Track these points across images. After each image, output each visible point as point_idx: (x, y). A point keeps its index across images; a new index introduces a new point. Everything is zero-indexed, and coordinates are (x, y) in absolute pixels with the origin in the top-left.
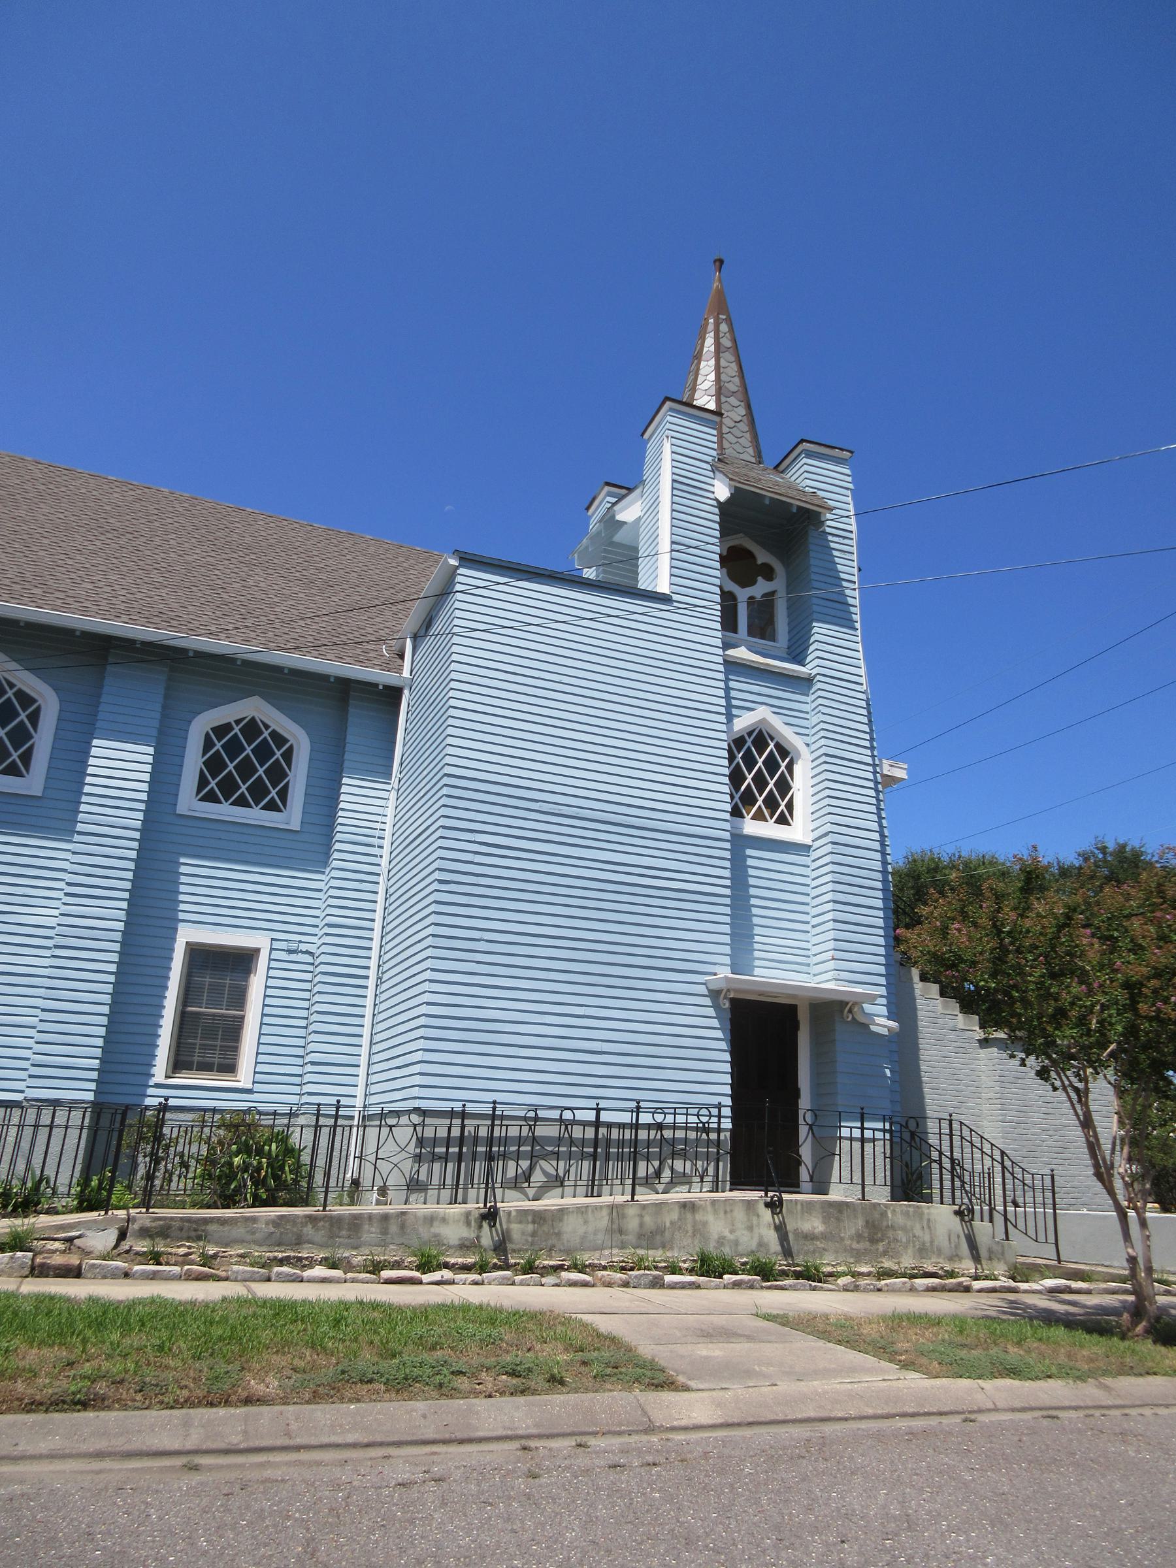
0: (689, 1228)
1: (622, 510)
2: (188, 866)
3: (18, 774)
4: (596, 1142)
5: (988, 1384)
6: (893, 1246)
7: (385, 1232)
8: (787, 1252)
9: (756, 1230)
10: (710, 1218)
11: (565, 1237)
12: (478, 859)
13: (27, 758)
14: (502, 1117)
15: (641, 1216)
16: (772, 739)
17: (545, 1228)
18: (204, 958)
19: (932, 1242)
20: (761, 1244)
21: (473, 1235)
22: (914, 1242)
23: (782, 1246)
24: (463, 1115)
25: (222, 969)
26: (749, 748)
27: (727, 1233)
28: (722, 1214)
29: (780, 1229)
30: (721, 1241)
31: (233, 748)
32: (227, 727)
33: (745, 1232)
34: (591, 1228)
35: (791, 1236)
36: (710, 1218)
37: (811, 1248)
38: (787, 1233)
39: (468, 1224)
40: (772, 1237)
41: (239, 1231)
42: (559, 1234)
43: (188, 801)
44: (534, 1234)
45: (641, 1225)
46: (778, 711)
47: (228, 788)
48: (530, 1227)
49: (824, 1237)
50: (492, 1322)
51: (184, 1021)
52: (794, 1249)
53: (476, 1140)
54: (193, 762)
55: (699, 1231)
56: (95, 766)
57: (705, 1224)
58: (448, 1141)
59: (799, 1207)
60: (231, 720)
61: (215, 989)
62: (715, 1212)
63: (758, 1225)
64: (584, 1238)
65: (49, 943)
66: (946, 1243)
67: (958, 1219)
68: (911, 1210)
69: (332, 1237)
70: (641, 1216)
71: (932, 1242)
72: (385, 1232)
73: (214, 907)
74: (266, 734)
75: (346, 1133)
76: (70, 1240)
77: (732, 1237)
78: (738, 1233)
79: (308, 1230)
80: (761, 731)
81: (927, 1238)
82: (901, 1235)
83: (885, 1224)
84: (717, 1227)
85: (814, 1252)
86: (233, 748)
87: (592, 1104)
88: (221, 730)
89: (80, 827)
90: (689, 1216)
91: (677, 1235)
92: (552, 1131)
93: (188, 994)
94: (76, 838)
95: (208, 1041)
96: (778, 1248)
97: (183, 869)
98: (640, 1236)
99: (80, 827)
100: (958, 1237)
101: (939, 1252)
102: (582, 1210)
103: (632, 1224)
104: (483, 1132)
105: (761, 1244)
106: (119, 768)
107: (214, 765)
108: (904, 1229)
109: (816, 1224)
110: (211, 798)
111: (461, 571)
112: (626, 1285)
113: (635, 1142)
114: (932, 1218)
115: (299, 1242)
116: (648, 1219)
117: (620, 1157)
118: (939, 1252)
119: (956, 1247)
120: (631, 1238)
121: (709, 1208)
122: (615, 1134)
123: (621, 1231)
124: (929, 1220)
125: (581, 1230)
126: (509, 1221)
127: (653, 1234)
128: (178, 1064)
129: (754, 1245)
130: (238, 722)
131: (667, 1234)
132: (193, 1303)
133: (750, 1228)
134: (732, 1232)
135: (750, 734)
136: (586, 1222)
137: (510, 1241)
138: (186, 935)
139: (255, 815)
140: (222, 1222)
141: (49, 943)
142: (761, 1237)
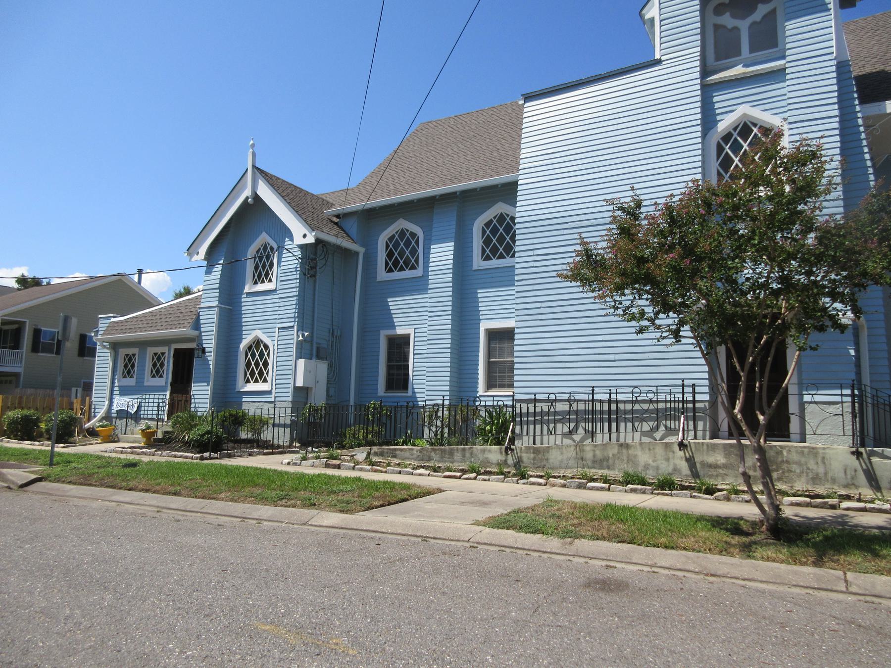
0: (625, 458)
1: (648, 12)
2: (482, 293)
3: (415, 268)
4: (610, 412)
5: (640, 553)
6: (787, 474)
7: (464, 456)
8: (695, 475)
9: (672, 461)
10: (639, 452)
11: (551, 461)
12: (537, 264)
13: (417, 261)
14: (575, 400)
15: (594, 451)
16: (755, 125)
17: (540, 456)
18: (494, 335)
19: (826, 474)
20: (676, 470)
21: (503, 459)
22: (807, 473)
23: (691, 471)
24: (535, 401)
25: (502, 338)
26: (736, 139)
27: (650, 462)
28: (647, 451)
29: (690, 461)
30: (646, 467)
31: (495, 231)
32: (491, 221)
33: (664, 462)
34: (565, 457)
35: (698, 466)
36: (639, 452)
37: (715, 473)
38: (695, 463)
39: (501, 453)
40: (684, 466)
41: (407, 454)
42: (547, 459)
43: (478, 262)
44: (534, 459)
45: (594, 456)
46: (755, 104)
47: (494, 251)
48: (532, 455)
49: (725, 466)
50: (26, 454)
51: (490, 366)
52: (701, 473)
53: (528, 414)
54: (477, 242)
55: (631, 460)
56: (433, 257)
57: (635, 456)
58: (528, 414)
59: (705, 447)
60: (492, 217)
61: (501, 350)
62: (642, 449)
63: (673, 458)
64: (561, 461)
65: (425, 339)
66: (842, 475)
67: (854, 457)
68: (806, 450)
69: (442, 457)
70: (594, 451)
71: (826, 474)
72: (464, 456)
73: (495, 311)
74: (508, 219)
75: (201, 405)
76: (352, 456)
77: (654, 464)
78: (659, 462)
79: (433, 454)
80: (745, 123)
81: (821, 470)
82: (794, 467)
83: (780, 459)
84: (644, 458)
85: (717, 476)
86: (495, 231)
87: (630, 390)
88: (391, 239)
89: (430, 286)
90: (624, 451)
91: (617, 462)
92: (565, 407)
93: (490, 353)
94: (430, 291)
95: (500, 374)
96: (689, 473)
97: (479, 295)
98: (594, 462)
99: (430, 286)
100: (856, 471)
101: (834, 481)
102: (560, 447)
103: (589, 455)
104: (531, 410)
105: (676, 470)
106: (442, 255)
107: (487, 242)
108: (799, 463)
109: (718, 459)
110: (488, 258)
111: (527, 105)
112: (564, 486)
113: (593, 412)
114: (827, 456)
115: (430, 459)
116: (598, 453)
117: (602, 420)
118: (834, 481)
119: (853, 478)
120: (590, 463)
121: (638, 447)
122: (621, 406)
123: (582, 459)
124: (824, 458)
125: (560, 458)
126: (521, 452)
127: (601, 461)
128: (490, 385)
129: (670, 470)
130: (495, 218)
131: (611, 461)
132: (265, 469)
133: (668, 460)
134: (653, 461)
135: (735, 129)
136: (562, 453)
137: (522, 462)
138: (484, 325)
139: (408, 274)
140: (401, 450)
141: (425, 339)
142: (675, 465)
